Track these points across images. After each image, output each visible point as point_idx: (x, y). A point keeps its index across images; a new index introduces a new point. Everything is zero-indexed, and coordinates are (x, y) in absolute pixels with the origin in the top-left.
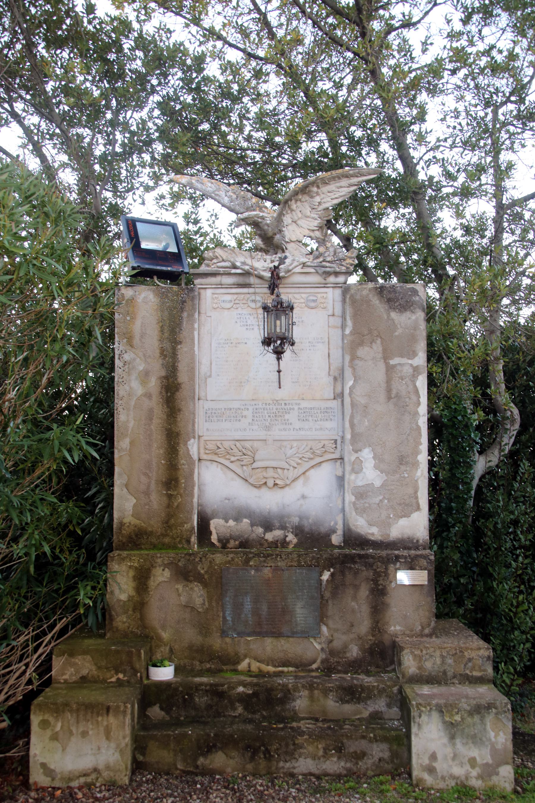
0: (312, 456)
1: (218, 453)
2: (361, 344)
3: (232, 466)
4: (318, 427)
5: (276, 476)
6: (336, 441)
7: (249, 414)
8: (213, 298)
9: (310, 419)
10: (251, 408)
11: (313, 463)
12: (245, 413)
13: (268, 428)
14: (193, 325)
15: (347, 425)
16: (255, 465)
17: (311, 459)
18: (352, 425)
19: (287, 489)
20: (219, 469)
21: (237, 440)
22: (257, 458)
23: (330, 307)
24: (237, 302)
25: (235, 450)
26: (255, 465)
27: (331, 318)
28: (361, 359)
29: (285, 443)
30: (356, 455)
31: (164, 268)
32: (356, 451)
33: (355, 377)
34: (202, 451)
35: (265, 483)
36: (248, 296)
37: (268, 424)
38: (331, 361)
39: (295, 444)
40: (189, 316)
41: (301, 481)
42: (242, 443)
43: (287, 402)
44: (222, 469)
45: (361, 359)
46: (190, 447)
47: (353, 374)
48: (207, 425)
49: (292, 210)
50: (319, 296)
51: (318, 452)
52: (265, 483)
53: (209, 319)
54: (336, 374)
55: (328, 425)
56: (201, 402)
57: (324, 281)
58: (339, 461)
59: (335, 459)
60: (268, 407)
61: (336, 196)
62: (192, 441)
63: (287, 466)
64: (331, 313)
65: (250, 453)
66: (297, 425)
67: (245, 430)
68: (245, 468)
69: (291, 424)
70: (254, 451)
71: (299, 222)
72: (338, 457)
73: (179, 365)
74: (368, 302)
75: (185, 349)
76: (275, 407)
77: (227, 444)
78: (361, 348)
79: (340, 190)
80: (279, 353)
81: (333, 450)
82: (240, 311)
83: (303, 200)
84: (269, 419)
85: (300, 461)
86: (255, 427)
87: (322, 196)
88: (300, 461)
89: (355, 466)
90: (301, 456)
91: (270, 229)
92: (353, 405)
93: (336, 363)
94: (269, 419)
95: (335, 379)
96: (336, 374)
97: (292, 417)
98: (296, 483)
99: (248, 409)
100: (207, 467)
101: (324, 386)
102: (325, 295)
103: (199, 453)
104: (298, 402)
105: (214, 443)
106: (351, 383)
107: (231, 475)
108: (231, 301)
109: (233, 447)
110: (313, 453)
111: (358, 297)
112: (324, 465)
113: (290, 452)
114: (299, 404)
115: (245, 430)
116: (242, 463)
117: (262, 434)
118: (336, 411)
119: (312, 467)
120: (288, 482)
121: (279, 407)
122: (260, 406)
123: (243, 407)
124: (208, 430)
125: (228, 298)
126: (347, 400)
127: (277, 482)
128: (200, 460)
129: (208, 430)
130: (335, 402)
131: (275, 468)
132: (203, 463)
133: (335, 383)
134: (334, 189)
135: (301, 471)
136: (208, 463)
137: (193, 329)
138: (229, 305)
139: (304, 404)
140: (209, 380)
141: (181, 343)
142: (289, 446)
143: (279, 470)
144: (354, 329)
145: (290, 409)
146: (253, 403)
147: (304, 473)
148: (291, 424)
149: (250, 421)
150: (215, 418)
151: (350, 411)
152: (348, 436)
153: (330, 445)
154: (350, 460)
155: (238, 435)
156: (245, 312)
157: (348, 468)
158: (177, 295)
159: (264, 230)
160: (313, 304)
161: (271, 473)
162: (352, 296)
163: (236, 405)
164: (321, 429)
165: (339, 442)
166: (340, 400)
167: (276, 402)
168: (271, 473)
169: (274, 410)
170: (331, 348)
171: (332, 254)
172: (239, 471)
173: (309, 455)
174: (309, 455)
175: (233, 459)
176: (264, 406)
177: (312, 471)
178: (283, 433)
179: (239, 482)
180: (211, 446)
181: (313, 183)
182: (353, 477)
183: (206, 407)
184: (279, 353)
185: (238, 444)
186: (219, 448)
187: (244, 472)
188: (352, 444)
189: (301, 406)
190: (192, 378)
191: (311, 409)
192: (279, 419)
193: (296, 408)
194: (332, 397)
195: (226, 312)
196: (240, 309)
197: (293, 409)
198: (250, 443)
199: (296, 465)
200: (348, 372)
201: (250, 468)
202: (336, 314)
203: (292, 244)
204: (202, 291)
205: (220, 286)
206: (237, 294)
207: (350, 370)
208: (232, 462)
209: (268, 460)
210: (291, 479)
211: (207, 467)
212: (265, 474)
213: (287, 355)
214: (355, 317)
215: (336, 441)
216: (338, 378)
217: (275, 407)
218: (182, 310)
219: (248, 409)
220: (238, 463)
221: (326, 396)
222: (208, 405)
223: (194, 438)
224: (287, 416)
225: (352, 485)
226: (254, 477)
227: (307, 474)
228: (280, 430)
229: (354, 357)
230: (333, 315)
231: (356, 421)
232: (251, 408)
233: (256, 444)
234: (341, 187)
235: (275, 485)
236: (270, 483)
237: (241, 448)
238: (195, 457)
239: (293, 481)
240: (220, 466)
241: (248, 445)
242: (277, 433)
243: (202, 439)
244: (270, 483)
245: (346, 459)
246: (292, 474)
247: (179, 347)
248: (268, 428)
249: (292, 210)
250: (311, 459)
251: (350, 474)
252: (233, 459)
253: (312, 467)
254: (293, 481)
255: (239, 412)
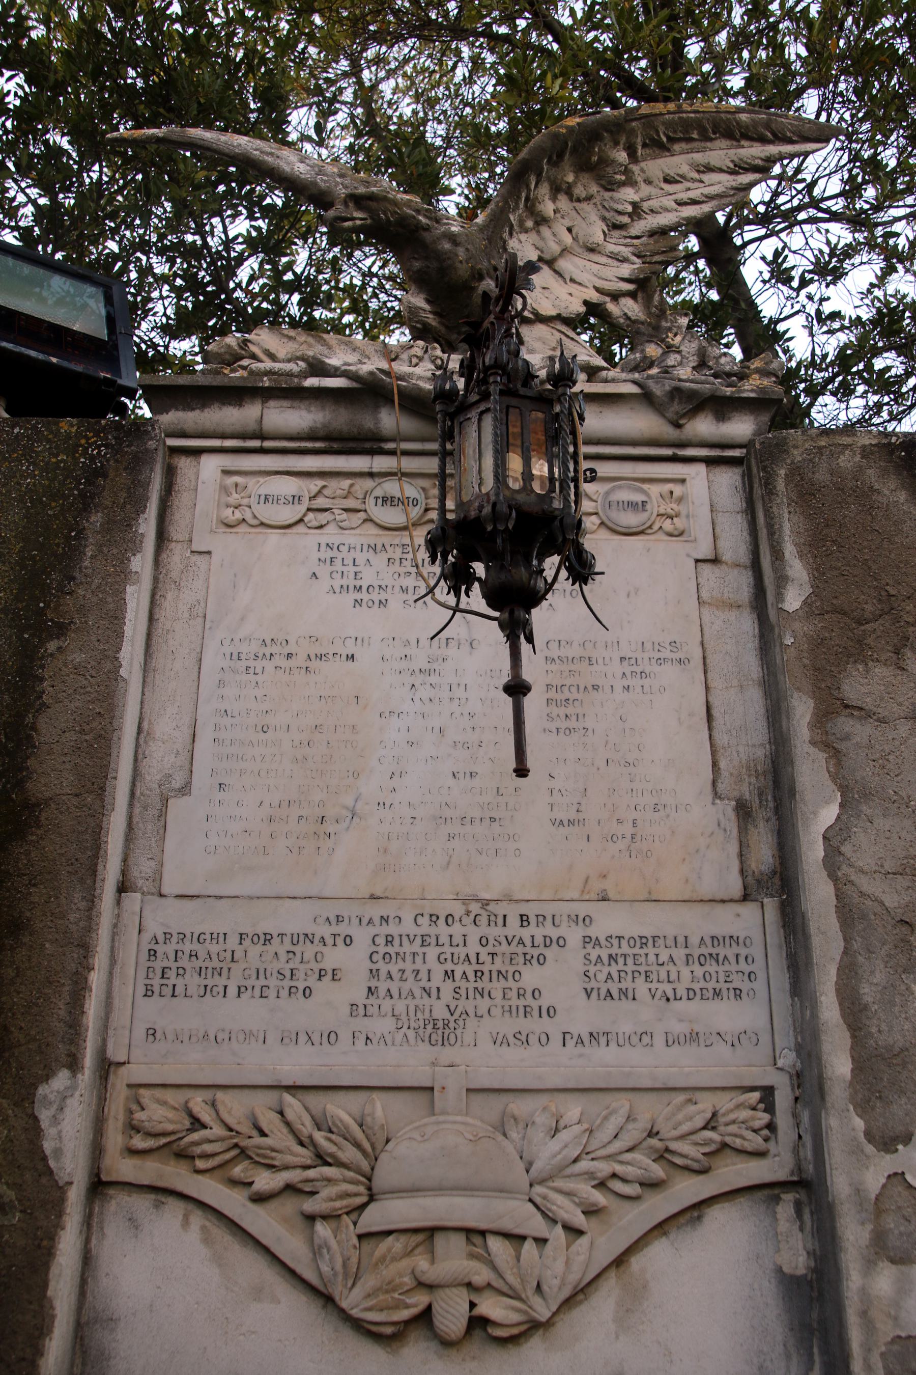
0: (658, 1171)
1: (189, 1153)
2: (858, 652)
3: (263, 1222)
4: (678, 1028)
5: (482, 1275)
6: (768, 1093)
7: (353, 960)
8: (224, 490)
9: (642, 988)
10: (362, 936)
11: (661, 1206)
12: (334, 957)
13: (441, 1032)
14: (124, 561)
15: (830, 1010)
16: (373, 1219)
17: (652, 1185)
18: (854, 1013)
19: (535, 1346)
20: (194, 1234)
21: (293, 1089)
22: (384, 1176)
23: (701, 528)
24: (321, 502)
25: (279, 1138)
26: (373, 1219)
27: (706, 569)
28: (862, 713)
29: (521, 1106)
30: (887, 1164)
31: (33, 353)
32: (887, 1142)
33: (844, 789)
34: (114, 1139)
35: (426, 1316)
36: (369, 483)
37: (440, 1012)
38: (722, 739)
39: (573, 1109)
40: (109, 527)
41: (604, 1303)
42: (316, 1101)
43: (531, 910)
44: (207, 1240)
45: (862, 713)
46: (44, 1116)
47: (834, 777)
48: (151, 1011)
49: (541, 221)
50: (655, 490)
51: (683, 1147)
52: (426, 1316)
53: (200, 560)
54: (746, 792)
55: (727, 1016)
56: (133, 900)
57: (669, 432)
58: (789, 1198)
59: (769, 1191)
60: (442, 929)
61: (692, 194)
62: (61, 1080)
63: (536, 1225)
64: (704, 550)
65: (349, 1154)
66: (582, 1016)
67: (331, 1037)
68: (322, 1230)
69: (551, 1012)
70: (373, 1146)
71: (564, 264)
72: (782, 1175)
73: (43, 722)
74: (865, 496)
75: (79, 657)
76: (474, 934)
77: (235, 1108)
78: (855, 671)
79: (706, 178)
80: (514, 605)
81: (755, 1142)
82: (331, 535)
83: (579, 191)
84: (447, 988)
85: (599, 1198)
86: (382, 1026)
87: (646, 190)
88: (599, 1198)
89: (890, 1222)
90: (604, 1168)
91: (461, 253)
92: (848, 914)
93: (747, 739)
94: (447, 988)
95: (743, 811)
96: (746, 792)
97: (558, 979)
98: (580, 1314)
99: (348, 941)
100: (134, 1224)
101: (699, 845)
102: (678, 490)
103: (97, 1150)
104: (582, 909)
105: (175, 1098)
106: (829, 814)
107: (250, 1267)
108: (296, 499)
109: (269, 1120)
110: (663, 1156)
111: (821, 476)
112: (717, 1215)
113: (548, 1151)
114: (587, 920)
115: (331, 1037)
116: (310, 1205)
117: (412, 1062)
118: (757, 951)
119: (661, 1228)
120: (543, 1312)
121: (495, 932)
122: (408, 927)
123: (326, 931)
124: (152, 1033)
125: (288, 486)
126: (818, 894)
127: (492, 1308)
128: (98, 1186)
129: (152, 1033)
130: (750, 911)
131: (474, 1234)
132: (119, 1204)
133: (743, 831)
134: (685, 169)
135: (603, 1244)
136: (141, 1204)
137: (124, 575)
138: (288, 514)
139: (610, 922)
140: (176, 806)
141: (61, 630)
142: (543, 1120)
143: (495, 1244)
144: (816, 592)
145: (548, 942)
146: (375, 911)
147: (620, 1261)
148: (551, 1012)
149: (360, 996)
150: (194, 982)
151: (838, 945)
152: (839, 1065)
153: (742, 1115)
154: (858, 1191)
155: (297, 1064)
156: (350, 538)
157: (854, 1234)
158: (72, 451)
159: (440, 257)
160: (631, 519)
161: (453, 1259)
162: (796, 472)
163: (295, 919)
164: (693, 1037)
165: (783, 1099)
166: (771, 904)
167: (483, 908)
168: (453, 1259)
169: (473, 947)
170: (716, 683)
171: (693, 361)
172: (292, 1247)
173: (643, 1164)
174: (643, 1164)
175: (265, 1181)
176: (425, 926)
177: (659, 1252)
178: (514, 1053)
179: (289, 1309)
180: (158, 1114)
181: (616, 130)
182: (884, 1281)
183: (154, 927)
184: (514, 605)
185: (293, 1105)
186: (197, 1124)
187: (316, 1250)
188: (863, 1107)
189: (598, 930)
190: (96, 784)
191: (643, 941)
192: (497, 987)
193: (574, 935)
194: (735, 886)
195: (274, 537)
196: (331, 529)
197: (561, 942)
198: (355, 1101)
199: (579, 1220)
200: (810, 770)
201: (349, 1231)
202: (727, 556)
203: (540, 330)
204: (184, 463)
205: (258, 441)
206: (322, 474)
207: (821, 756)
208: (260, 1199)
209: (439, 1189)
210: (557, 1293)
211: (134, 1224)
212: (422, 1263)
213: (557, 615)
214: (816, 547)
215: (768, 1093)
216: (770, 797)
217: (474, 934)
218: (86, 503)
219: (348, 941)
220: (290, 1206)
221: (709, 886)
222: (163, 917)
223: (74, 1064)
224: (531, 977)
225: (886, 1331)
226: (369, 1282)
227: (636, 1262)
228: (499, 1041)
229: (832, 707)
230: (715, 561)
231: (868, 993)
232: (362, 936)
233: (380, 1108)
234: (709, 169)
235: (478, 1323)
236: (452, 1315)
237: (307, 1127)
238: (70, 1162)
239: (569, 1303)
240: (198, 1219)
241: (341, 1110)
242: (484, 1056)
243: (120, 1080)
244: (452, 1315)
245: (840, 1184)
246: (560, 1264)
247: (52, 646)
248: (441, 1032)
249: (541, 221)
250: (652, 1185)
251: (869, 1265)
252: (265, 1181)
253: (661, 1228)
254: (569, 1303)
255: (309, 950)
